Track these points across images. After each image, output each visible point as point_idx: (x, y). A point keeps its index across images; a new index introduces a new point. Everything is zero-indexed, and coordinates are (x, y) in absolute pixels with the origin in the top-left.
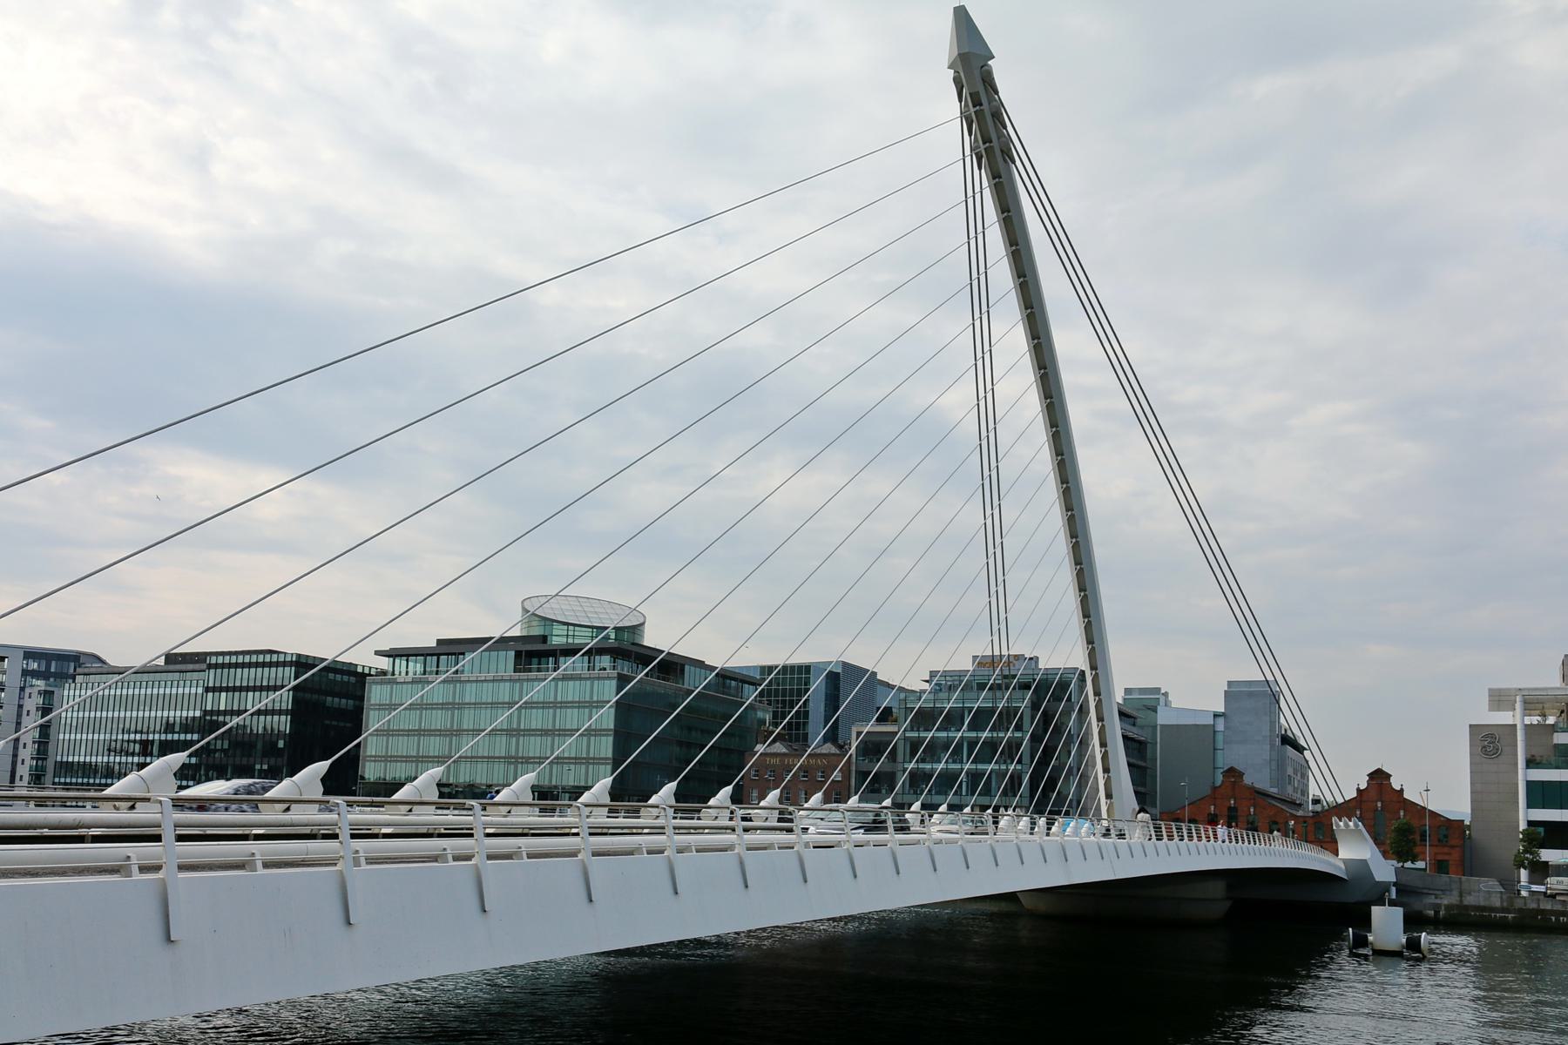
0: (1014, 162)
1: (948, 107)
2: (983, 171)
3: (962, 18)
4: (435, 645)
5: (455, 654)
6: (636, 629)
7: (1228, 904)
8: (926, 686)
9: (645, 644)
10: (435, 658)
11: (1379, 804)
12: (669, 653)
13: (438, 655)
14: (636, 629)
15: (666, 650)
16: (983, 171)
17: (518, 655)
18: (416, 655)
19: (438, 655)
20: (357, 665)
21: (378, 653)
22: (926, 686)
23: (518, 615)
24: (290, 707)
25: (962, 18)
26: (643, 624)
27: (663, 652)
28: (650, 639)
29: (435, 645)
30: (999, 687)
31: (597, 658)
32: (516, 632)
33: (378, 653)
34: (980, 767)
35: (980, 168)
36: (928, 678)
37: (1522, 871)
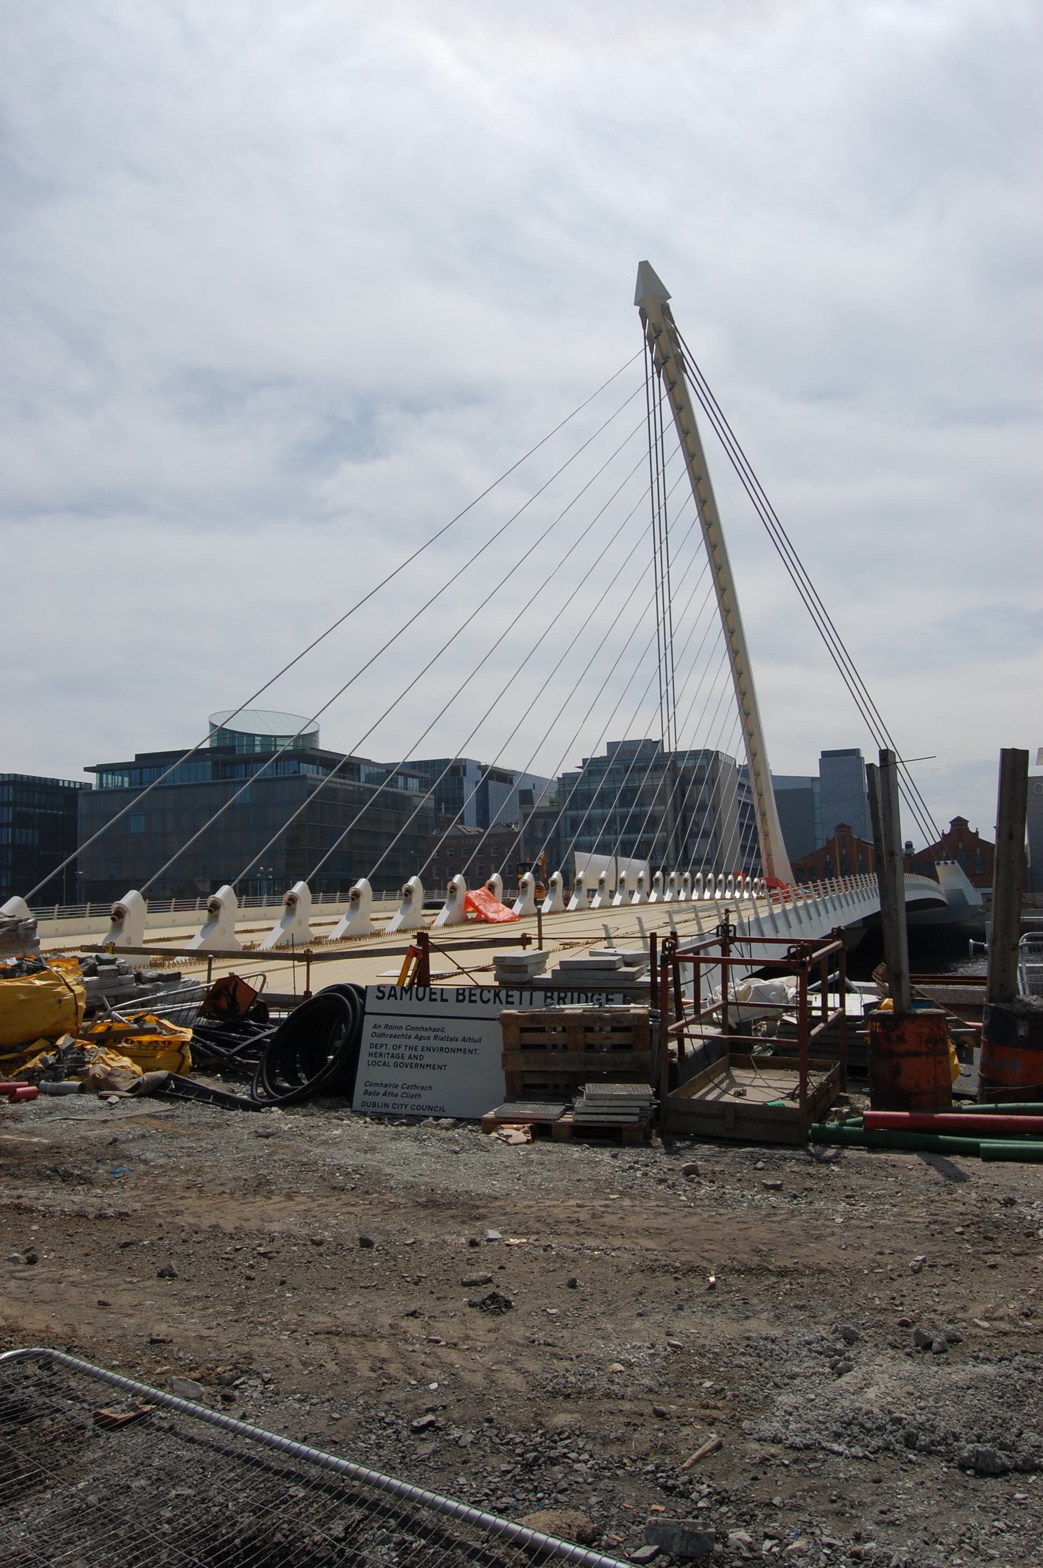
0: (686, 372)
1: (635, 333)
2: (661, 379)
3: (645, 269)
4: (133, 760)
5: (157, 767)
6: (314, 735)
7: (865, 931)
8: (581, 770)
9: (321, 748)
10: (138, 771)
11: (960, 845)
12: (350, 757)
13: (141, 768)
14: (314, 735)
15: (348, 754)
16: (661, 379)
17: (215, 764)
18: (121, 770)
19: (141, 768)
20: (58, 780)
21: (86, 769)
22: (581, 770)
23: (206, 732)
24: (10, 821)
25: (645, 269)
26: (317, 732)
27: (345, 756)
28: (326, 744)
29: (133, 760)
30: (618, 771)
31: (254, 765)
32: (206, 745)
33: (86, 769)
34: (632, 836)
35: (659, 377)
36: (581, 765)
37: (702, 1013)
